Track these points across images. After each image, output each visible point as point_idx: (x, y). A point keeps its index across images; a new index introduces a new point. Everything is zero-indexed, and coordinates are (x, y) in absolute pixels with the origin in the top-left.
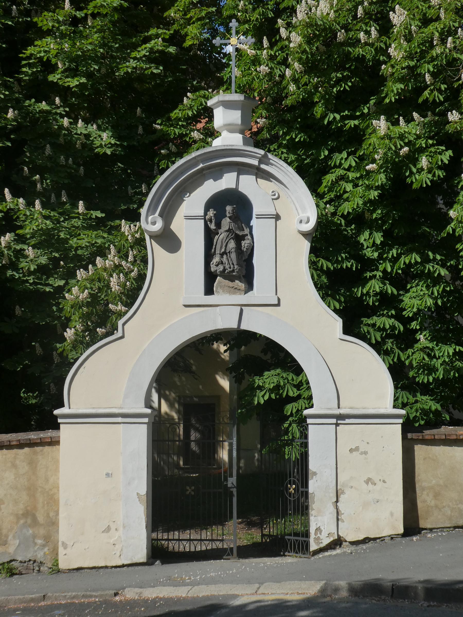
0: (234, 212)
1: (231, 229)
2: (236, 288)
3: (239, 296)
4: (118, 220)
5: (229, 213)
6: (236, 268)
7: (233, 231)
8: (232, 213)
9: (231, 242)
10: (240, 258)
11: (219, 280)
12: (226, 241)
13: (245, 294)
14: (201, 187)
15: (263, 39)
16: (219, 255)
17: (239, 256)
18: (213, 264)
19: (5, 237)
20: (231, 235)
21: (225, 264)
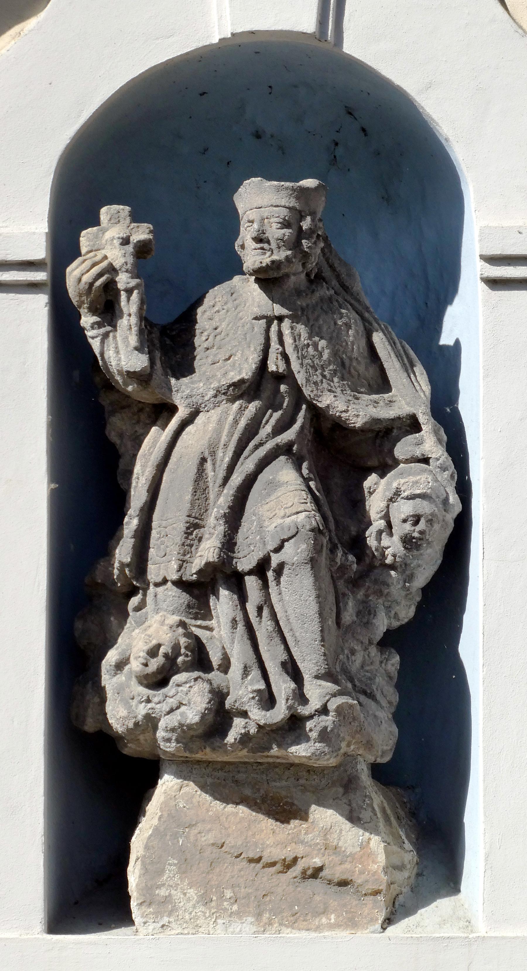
0: (300, 234)
1: (279, 378)
2: (316, 872)
3: (343, 934)
4: (400, 658)
5: (259, 239)
6: (315, 704)
7: (297, 390)
8: (283, 243)
9: (273, 485)
10: (349, 616)
11: (171, 798)
12: (237, 479)
13: (389, 921)
14: (31, 23)
15: (273, 323)
16: (170, 591)
17: (339, 599)
18: (120, 666)
19: (348, 612)
20: (280, 429)
21: (225, 666)
